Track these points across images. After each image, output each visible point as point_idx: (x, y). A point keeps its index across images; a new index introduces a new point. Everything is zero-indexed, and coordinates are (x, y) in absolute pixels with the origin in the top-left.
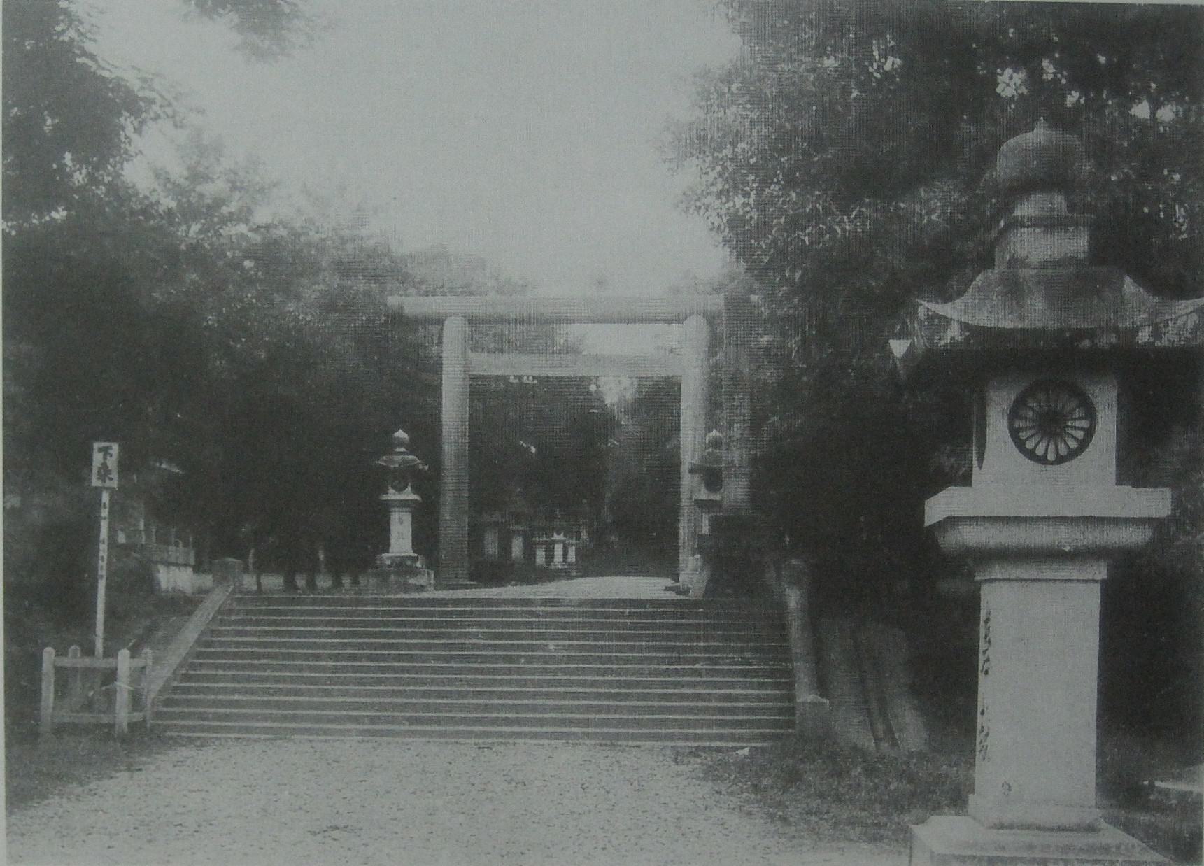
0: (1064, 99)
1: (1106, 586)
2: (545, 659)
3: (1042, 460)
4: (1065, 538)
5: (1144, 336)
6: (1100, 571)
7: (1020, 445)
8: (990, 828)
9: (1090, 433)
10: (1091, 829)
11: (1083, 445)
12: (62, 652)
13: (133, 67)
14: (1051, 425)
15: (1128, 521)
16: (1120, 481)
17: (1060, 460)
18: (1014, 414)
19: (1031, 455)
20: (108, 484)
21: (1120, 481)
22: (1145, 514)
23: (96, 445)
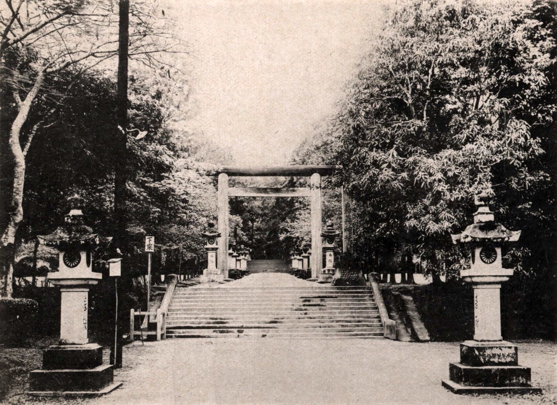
0: (425, 287)
1: (500, 289)
2: (366, 308)
3: (487, 263)
4: (492, 279)
5: (506, 239)
6: (500, 286)
7: (482, 260)
8: (217, 189)
9: (496, 257)
10: (500, 340)
11: (495, 260)
12: (136, 311)
13: (533, 400)
14: (488, 257)
15: (503, 276)
16: (503, 267)
17: (490, 263)
18: (481, 254)
19: (484, 262)
20: (151, 251)
21: (503, 267)
22: (507, 274)
23: (147, 237)
